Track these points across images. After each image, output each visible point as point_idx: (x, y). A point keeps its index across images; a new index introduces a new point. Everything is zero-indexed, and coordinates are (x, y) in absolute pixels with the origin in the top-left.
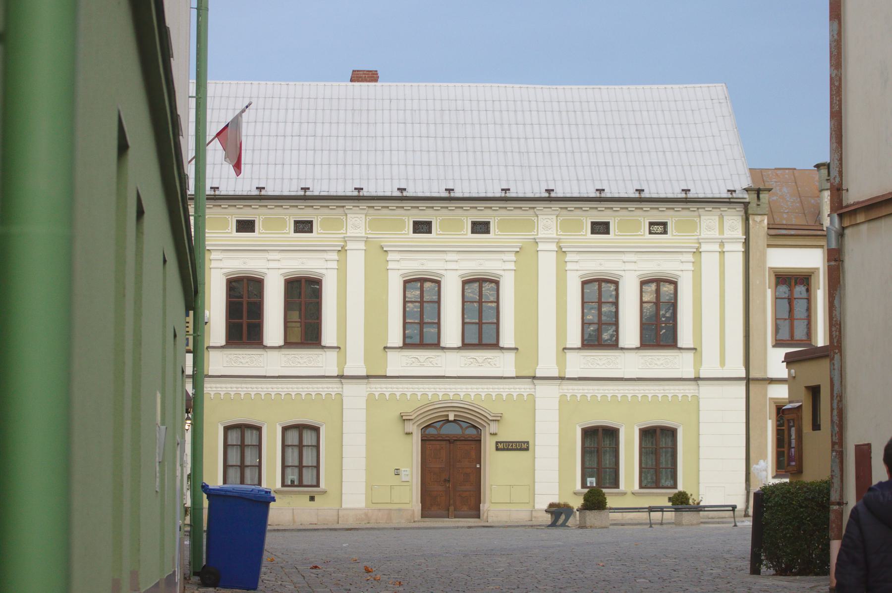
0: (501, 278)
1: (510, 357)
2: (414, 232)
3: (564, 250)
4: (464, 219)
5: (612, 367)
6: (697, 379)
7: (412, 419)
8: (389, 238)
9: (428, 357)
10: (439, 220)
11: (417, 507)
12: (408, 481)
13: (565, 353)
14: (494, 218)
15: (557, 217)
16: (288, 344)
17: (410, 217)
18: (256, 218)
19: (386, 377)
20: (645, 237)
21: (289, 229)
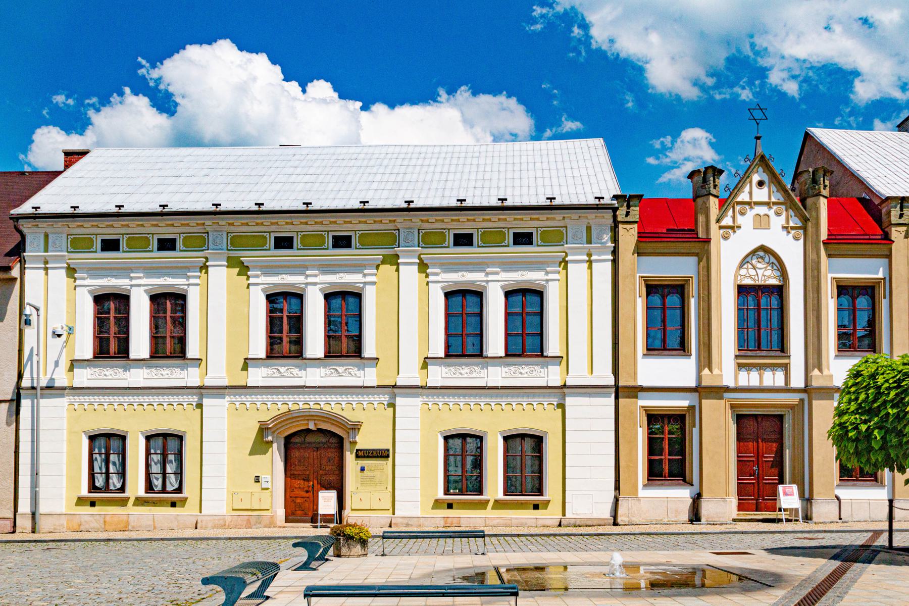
14: (478, 231)
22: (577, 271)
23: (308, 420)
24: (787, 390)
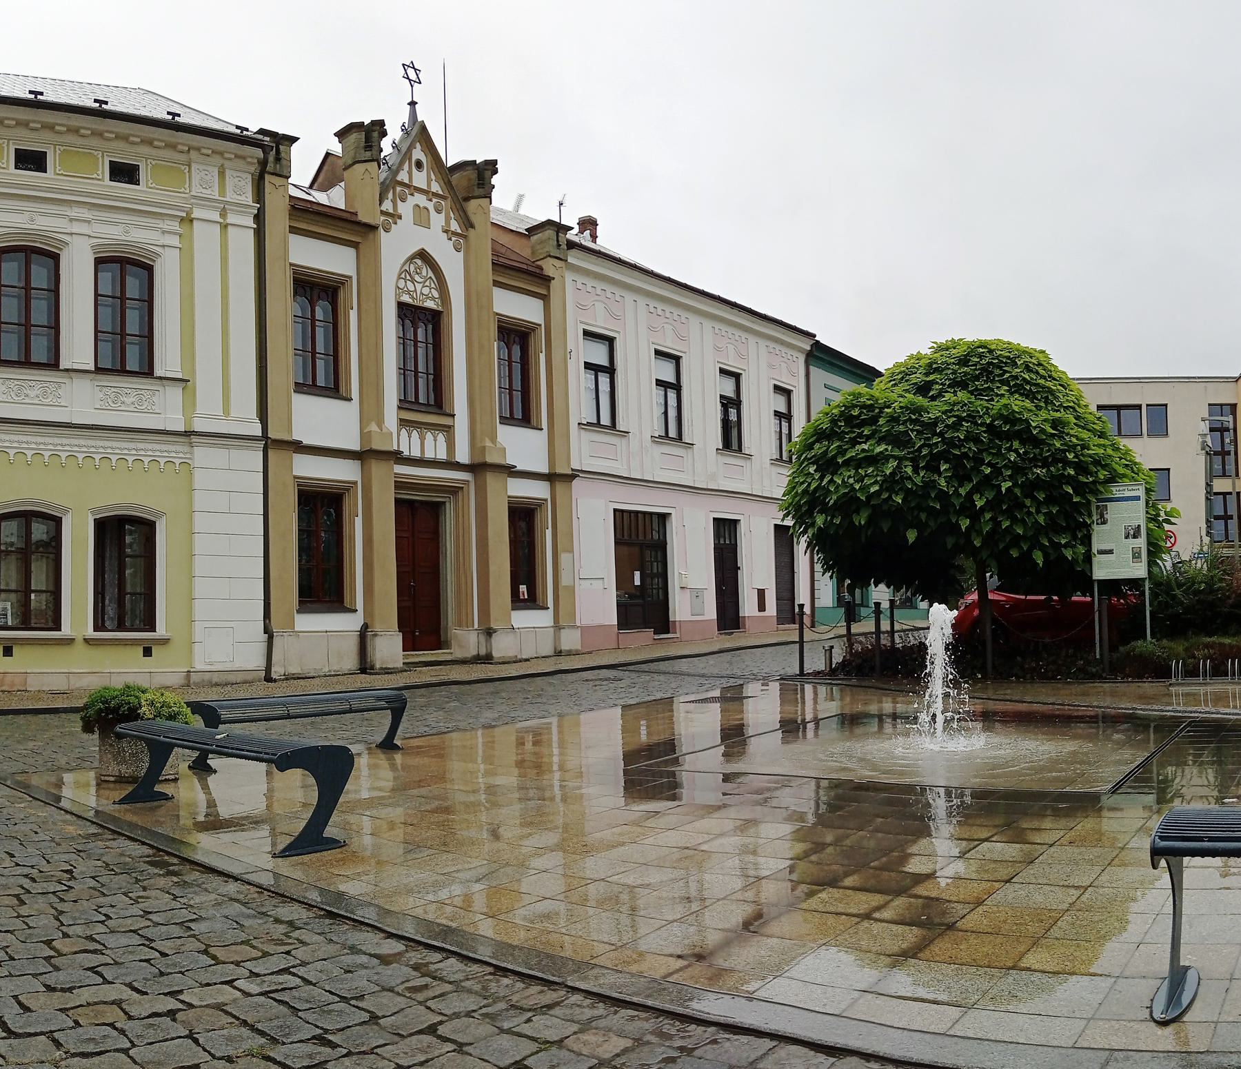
0: (159, 261)
5: (146, 410)
6: (188, 434)
14: (55, 148)
22: (205, 236)
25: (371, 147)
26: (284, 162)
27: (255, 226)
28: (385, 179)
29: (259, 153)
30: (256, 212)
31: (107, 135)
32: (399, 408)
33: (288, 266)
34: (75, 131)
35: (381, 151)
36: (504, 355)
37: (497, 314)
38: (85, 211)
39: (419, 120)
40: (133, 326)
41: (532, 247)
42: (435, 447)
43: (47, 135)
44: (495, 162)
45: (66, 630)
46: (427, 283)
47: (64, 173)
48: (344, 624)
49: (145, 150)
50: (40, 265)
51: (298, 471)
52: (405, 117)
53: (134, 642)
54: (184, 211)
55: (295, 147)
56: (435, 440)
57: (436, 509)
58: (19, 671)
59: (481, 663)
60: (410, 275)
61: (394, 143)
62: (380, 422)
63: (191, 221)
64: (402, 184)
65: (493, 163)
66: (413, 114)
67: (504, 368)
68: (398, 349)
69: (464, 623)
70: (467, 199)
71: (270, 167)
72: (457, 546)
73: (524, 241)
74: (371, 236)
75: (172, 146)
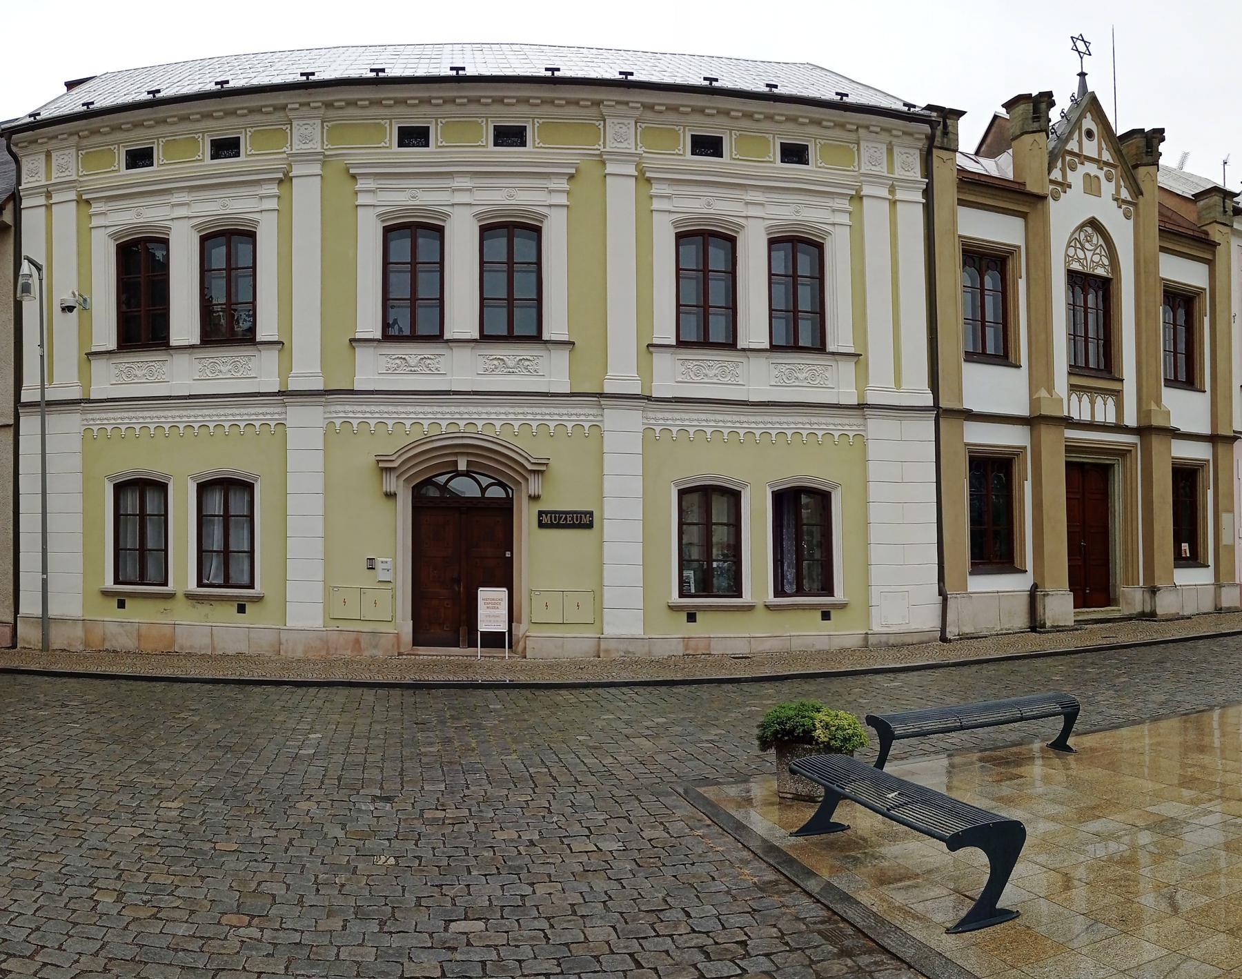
1: (560, 358)
2: (496, 144)
3: (648, 175)
4: (482, 122)
5: (730, 382)
6: (861, 406)
7: (394, 468)
8: (360, 154)
9: (521, 358)
10: (440, 125)
11: (406, 628)
12: (390, 582)
13: (651, 353)
14: (533, 121)
15: (636, 123)
16: (390, 336)
17: (393, 120)
18: (430, 122)
19: (352, 392)
20: (489, 149)
21: (390, 140)
22: (875, 213)
23: (456, 454)
24: (1119, 428)
25: (1039, 117)
26: (951, 136)
27: (924, 201)
28: (1054, 148)
29: (926, 128)
30: (925, 187)
31: (777, 118)
32: (1069, 373)
33: (957, 238)
34: (749, 116)
35: (1050, 121)
36: (1169, 318)
37: (1163, 279)
38: (665, 186)
39: (1090, 90)
40: (805, 303)
41: (1199, 213)
42: (1105, 411)
43: (523, 109)
44: (1162, 131)
45: (747, 597)
46: (1098, 251)
47: (740, 158)
48: (1014, 584)
49: (814, 130)
50: (716, 247)
51: (969, 438)
52: (1074, 87)
53: (812, 607)
54: (853, 189)
55: (962, 121)
56: (1105, 404)
57: (1104, 471)
58: (703, 636)
59: (1147, 620)
60: (1080, 243)
61: (1063, 112)
62: (1050, 388)
63: (861, 198)
64: (1071, 153)
65: (1160, 132)
66: (1083, 85)
67: (1170, 331)
68: (1067, 315)
69: (1131, 581)
70: (1136, 167)
71: (937, 142)
72: (1125, 508)
73: (1190, 206)
74: (1040, 206)
75: (842, 126)
